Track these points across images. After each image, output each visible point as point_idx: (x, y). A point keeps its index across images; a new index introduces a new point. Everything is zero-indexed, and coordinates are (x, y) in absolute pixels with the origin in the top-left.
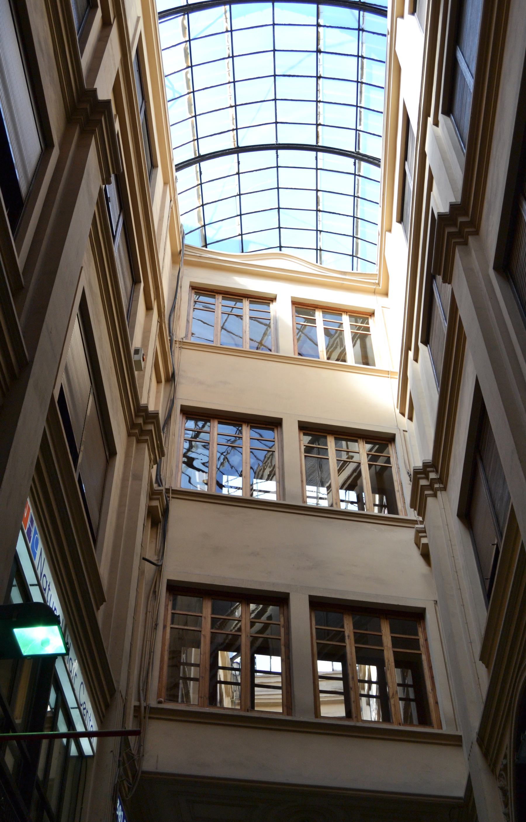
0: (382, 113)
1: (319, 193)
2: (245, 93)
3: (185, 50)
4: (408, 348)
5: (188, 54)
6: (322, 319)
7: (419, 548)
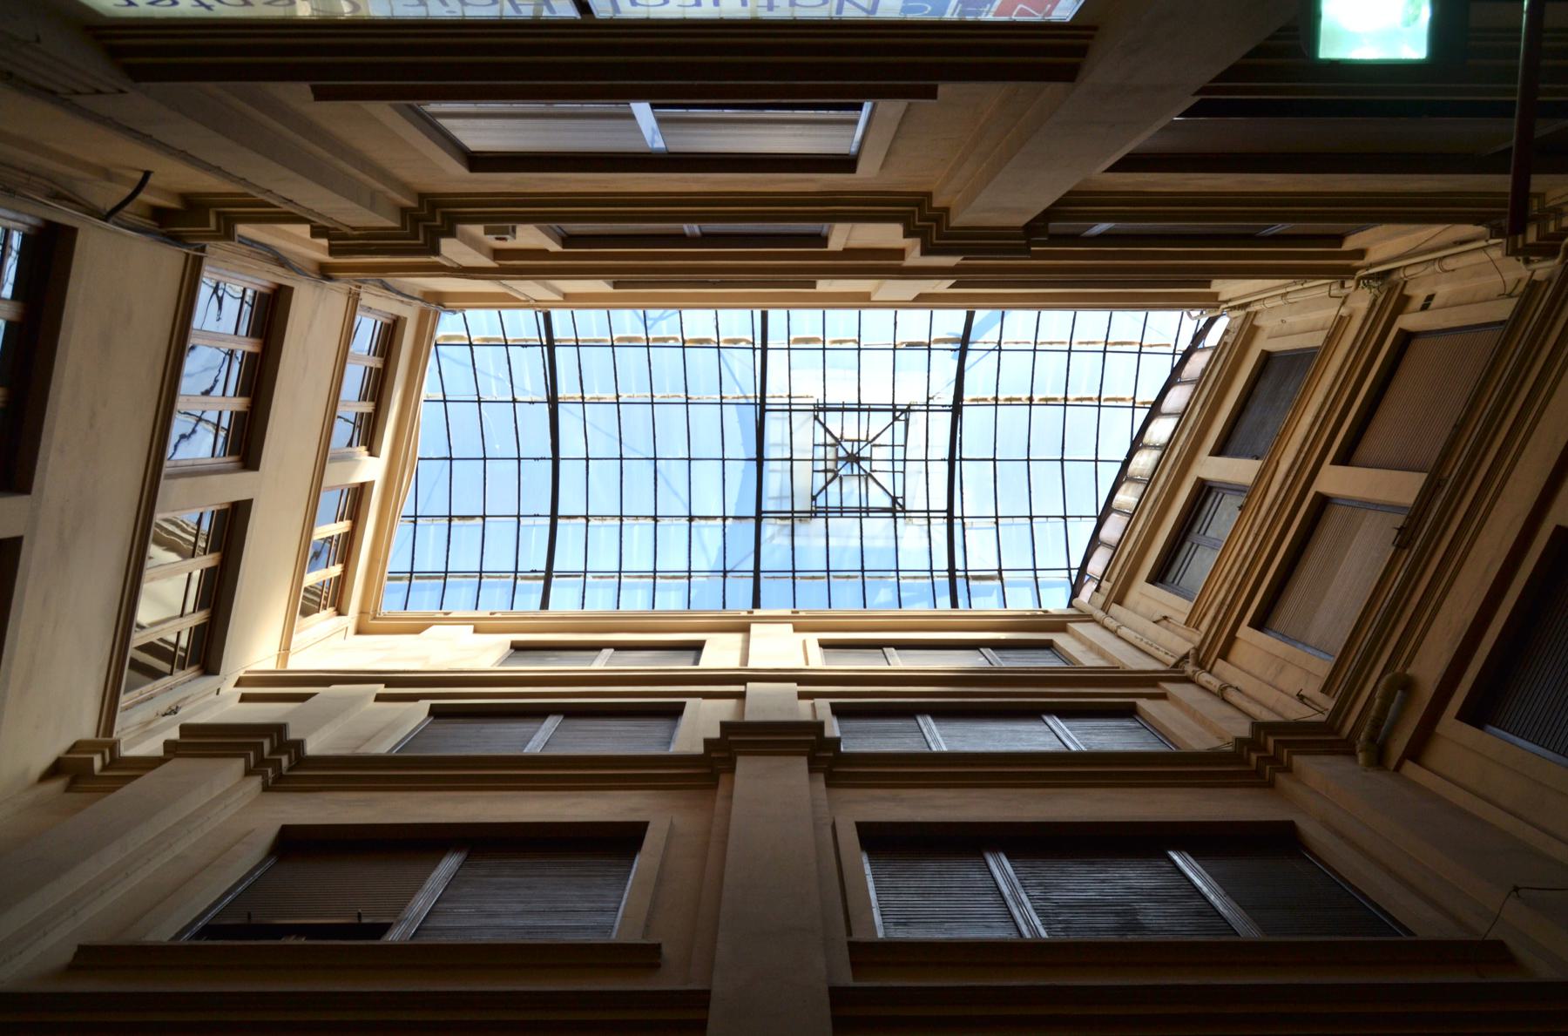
1: (479, 521)
2: (637, 417)
3: (707, 341)
5: (701, 343)
6: (335, 533)
7: (69, 751)
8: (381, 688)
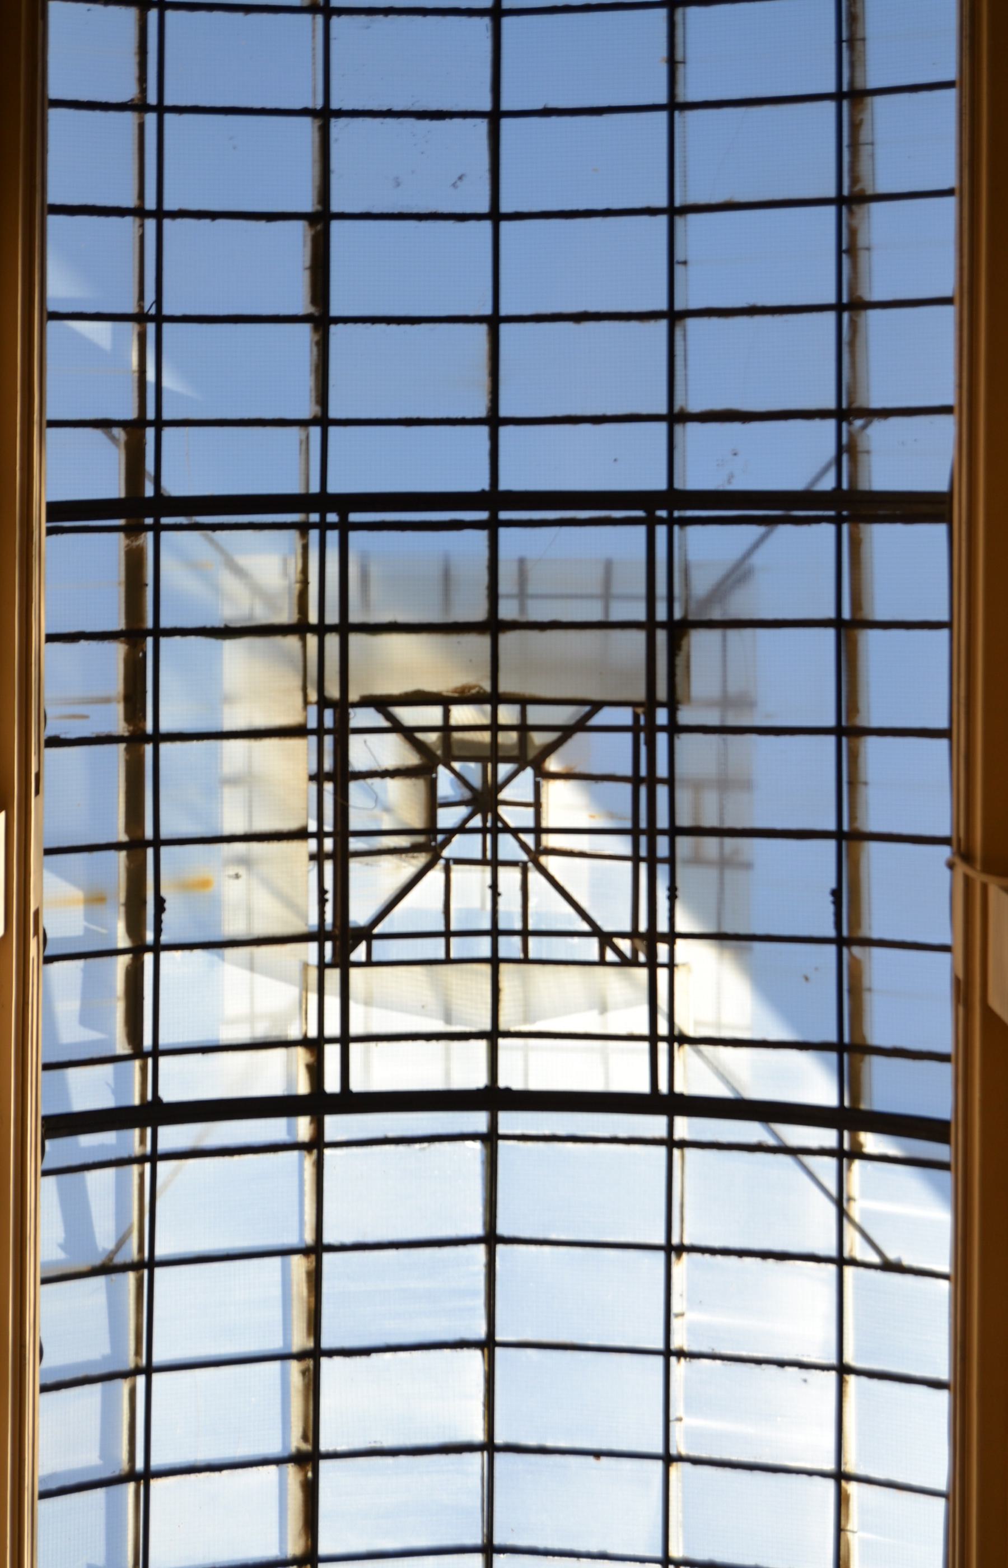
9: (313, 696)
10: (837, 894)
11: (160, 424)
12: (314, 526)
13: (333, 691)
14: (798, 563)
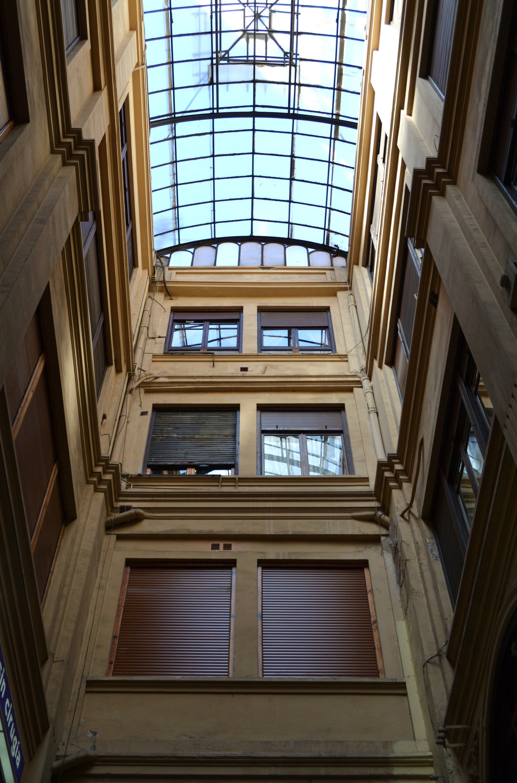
0: (359, 94)
4: (401, 107)
8: (404, 113)
9: (298, 68)
10: (172, 22)
11: (330, 138)
12: (296, 109)
13: (293, 68)
14: (184, 102)
